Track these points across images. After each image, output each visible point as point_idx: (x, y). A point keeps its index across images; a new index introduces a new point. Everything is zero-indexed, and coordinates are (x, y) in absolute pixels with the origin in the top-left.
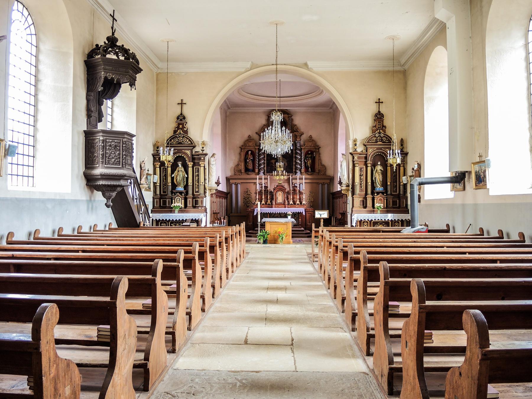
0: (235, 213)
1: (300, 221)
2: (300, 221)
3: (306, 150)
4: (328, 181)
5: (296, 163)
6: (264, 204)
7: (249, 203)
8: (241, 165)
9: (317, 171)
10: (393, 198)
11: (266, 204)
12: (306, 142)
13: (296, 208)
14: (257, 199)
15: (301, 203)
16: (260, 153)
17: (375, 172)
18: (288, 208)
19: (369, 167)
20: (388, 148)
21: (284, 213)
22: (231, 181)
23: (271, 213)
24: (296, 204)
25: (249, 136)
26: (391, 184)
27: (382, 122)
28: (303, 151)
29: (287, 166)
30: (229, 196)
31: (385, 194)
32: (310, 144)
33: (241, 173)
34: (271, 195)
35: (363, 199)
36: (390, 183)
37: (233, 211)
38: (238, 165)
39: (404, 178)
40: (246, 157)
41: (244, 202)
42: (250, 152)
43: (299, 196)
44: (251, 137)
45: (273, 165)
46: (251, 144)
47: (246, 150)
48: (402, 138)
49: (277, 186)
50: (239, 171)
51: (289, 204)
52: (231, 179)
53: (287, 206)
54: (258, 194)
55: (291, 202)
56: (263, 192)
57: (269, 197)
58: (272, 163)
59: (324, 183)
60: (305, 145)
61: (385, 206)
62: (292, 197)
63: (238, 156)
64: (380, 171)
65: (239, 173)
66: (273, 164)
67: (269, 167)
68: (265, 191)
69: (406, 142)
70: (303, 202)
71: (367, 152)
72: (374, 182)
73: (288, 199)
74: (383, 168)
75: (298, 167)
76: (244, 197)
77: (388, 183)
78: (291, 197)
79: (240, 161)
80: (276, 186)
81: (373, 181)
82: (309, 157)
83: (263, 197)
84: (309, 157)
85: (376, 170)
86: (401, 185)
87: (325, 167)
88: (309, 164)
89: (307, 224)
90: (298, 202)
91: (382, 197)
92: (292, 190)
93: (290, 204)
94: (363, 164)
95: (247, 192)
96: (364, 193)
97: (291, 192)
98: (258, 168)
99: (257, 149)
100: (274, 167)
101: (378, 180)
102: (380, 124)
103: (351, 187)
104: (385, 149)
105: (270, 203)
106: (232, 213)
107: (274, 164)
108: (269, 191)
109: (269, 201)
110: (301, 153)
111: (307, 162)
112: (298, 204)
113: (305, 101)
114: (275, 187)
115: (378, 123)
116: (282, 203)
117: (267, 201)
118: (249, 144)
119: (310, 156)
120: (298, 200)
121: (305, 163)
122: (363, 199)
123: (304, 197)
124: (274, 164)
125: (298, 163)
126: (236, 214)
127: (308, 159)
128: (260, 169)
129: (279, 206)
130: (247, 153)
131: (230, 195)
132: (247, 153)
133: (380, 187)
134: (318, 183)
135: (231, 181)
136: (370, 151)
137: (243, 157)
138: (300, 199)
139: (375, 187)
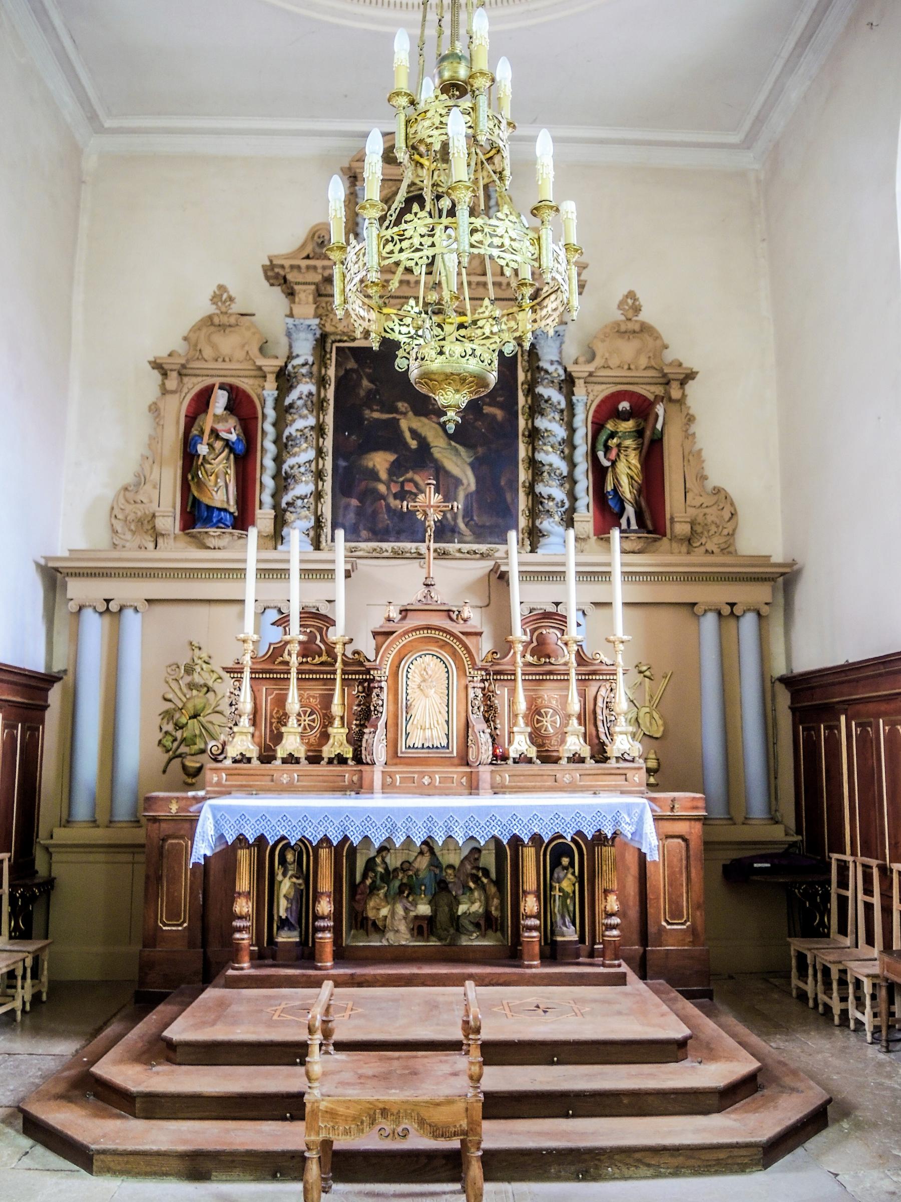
0: (94, 823)
1: (610, 915)
2: (610, 915)
3: (602, 392)
4: (760, 594)
5: (535, 465)
6: (297, 761)
7: (203, 751)
8: (158, 486)
9: (682, 529)
11: (267, 757)
12: (603, 341)
13: (562, 789)
14: (245, 722)
15: (600, 754)
16: (288, 401)
22: (77, 590)
23: (346, 838)
24: (556, 760)
25: (221, 296)
28: (580, 393)
29: (478, 491)
30: (55, 695)
32: (628, 349)
33: (157, 536)
34: (361, 682)
37: (82, 811)
38: (141, 480)
40: (195, 432)
41: (168, 742)
42: (220, 400)
43: (583, 695)
44: (231, 299)
45: (382, 488)
46: (228, 343)
47: (194, 385)
49: (405, 612)
50: (140, 521)
52: (79, 574)
53: (485, 772)
54: (247, 675)
55: (521, 745)
56: (294, 661)
57: (337, 699)
58: (373, 475)
59: (732, 605)
60: (592, 357)
63: (142, 426)
65: (137, 540)
66: (379, 480)
67: (354, 502)
68: (307, 650)
70: (618, 739)
73: (490, 714)
75: (550, 498)
76: (169, 706)
78: (522, 705)
79: (152, 457)
80: (395, 614)
82: (625, 435)
83: (293, 703)
84: (625, 435)
87: (732, 504)
88: (624, 481)
89: (652, 929)
90: (575, 744)
92: (527, 645)
93: (513, 754)
95: (189, 670)
97: (519, 660)
98: (276, 506)
99: (271, 378)
100: (383, 497)
105: (348, 753)
106: (68, 822)
107: (384, 475)
108: (339, 649)
109: (338, 732)
110: (571, 405)
111: (614, 463)
112: (577, 759)
113: (355, 1092)
114: (389, 620)
116: (445, 753)
117: (325, 736)
118: (214, 346)
119: (628, 425)
120: (574, 722)
121: (599, 473)
123: (622, 704)
124: (384, 475)
125: (552, 470)
126: (99, 835)
127: (619, 446)
128: (285, 511)
129: (423, 775)
130: (203, 400)
131: (64, 690)
132: (203, 400)
134: (694, 604)
135: (77, 590)
137: (173, 434)
138: (589, 717)
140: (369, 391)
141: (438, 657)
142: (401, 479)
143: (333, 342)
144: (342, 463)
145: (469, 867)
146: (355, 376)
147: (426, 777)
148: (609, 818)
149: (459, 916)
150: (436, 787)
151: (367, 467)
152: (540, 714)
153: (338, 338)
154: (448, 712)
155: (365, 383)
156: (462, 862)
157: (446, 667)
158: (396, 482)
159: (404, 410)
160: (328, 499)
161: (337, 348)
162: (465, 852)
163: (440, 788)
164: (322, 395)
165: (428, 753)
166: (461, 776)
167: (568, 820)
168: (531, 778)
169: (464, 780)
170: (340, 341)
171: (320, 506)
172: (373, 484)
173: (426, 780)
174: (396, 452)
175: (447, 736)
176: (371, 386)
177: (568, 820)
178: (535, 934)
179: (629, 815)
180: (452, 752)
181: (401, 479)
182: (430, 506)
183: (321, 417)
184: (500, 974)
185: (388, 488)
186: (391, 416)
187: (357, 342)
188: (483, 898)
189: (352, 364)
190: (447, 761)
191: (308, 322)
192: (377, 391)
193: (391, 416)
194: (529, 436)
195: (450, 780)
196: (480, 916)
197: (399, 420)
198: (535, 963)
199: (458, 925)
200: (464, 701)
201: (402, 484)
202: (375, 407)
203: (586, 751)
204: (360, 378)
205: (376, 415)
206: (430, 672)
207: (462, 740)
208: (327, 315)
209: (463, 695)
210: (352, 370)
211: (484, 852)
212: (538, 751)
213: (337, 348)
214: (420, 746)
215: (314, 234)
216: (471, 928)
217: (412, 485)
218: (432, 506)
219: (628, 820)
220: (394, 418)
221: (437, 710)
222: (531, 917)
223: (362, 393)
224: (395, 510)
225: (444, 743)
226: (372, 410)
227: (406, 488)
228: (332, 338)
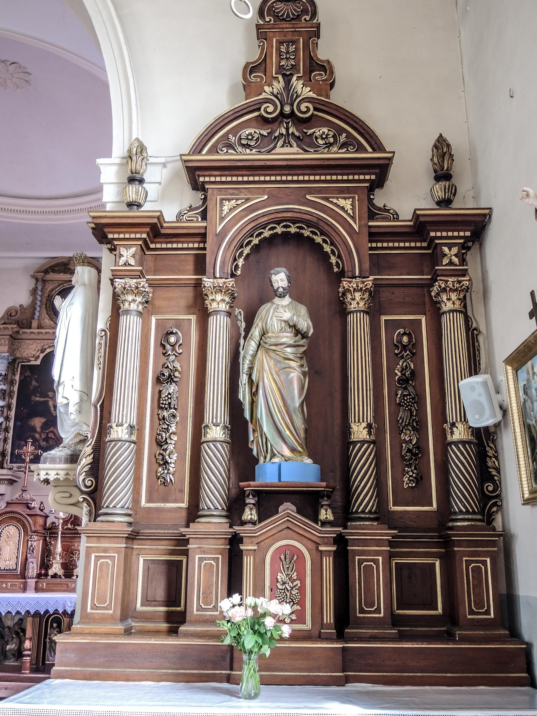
10: (391, 544)
17: (253, 345)
18: (37, 590)
19: (216, 312)
20: (348, 190)
21: (18, 613)
26: (380, 431)
27: (306, 45)
31: (325, 514)
35: (172, 553)
36: (369, 426)
39: (473, 389)
48: (441, 135)
51: (46, 575)
53: (31, 582)
58: (34, 429)
61: (329, 617)
62: (63, 546)
64: (287, 337)
69: (473, 160)
71: (204, 216)
72: (247, 415)
74: (313, 316)
77: (355, 427)
81: (242, 411)
85: (263, 334)
86: (456, 443)
91: (274, 538)
94: (183, 303)
96: (184, 505)
101: (275, 402)
102: (292, 48)
103: (85, 461)
104: (327, 199)
107: (39, 430)
115: (280, 43)
122: (172, 553)
124: (39, 430)
133: (287, 452)
136: (226, 209)
139: (257, 461)
140: (35, 387)
141: (16, 526)
142: (47, 431)
143: (20, 362)
144: (19, 423)
145: (16, 627)
146: (29, 379)
147: (4, 584)
148: (61, 604)
149: (6, 651)
150: (8, 589)
151: (31, 425)
152: (73, 554)
153: (21, 360)
154: (18, 553)
155: (34, 383)
156: (14, 625)
157: (19, 531)
158: (45, 433)
159: (51, 396)
160: (10, 441)
161: (21, 365)
162: (16, 620)
163: (10, 589)
164: (12, 389)
165: (7, 572)
166: (20, 583)
167: (43, 604)
168: (56, 585)
169: (21, 586)
170: (22, 362)
171: (5, 445)
172: (33, 434)
173: (4, 586)
174: (45, 417)
175: (16, 564)
176: (36, 384)
177: (43, 604)
178: (28, 658)
179: (71, 603)
180: (17, 572)
181: (47, 431)
182: (28, 452)
183: (10, 400)
184: (8, 676)
185: (40, 436)
186: (45, 399)
187: (31, 362)
188: (18, 642)
189: (28, 373)
190: (16, 576)
191: (3, 354)
192: (39, 386)
193: (45, 399)
194: (155, 237)
195: (15, 586)
196: (15, 651)
197: (48, 401)
198: (27, 672)
199: (5, 655)
200: (26, 547)
201: (48, 434)
202: (37, 395)
203: (60, 572)
204: (31, 380)
205: (38, 399)
206: (11, 534)
207: (23, 566)
208: (18, 349)
209: (26, 544)
210: (28, 376)
211: (24, 620)
212: (65, 572)
213: (21, 365)
214: (3, 569)
215: (8, 312)
216: (11, 656)
217: (52, 434)
218: (29, 452)
219: (70, 605)
220: (47, 400)
221: (13, 552)
222: (27, 650)
223: (32, 388)
224: (43, 447)
225: (14, 568)
226: (36, 397)
227: (49, 436)
228: (18, 361)
